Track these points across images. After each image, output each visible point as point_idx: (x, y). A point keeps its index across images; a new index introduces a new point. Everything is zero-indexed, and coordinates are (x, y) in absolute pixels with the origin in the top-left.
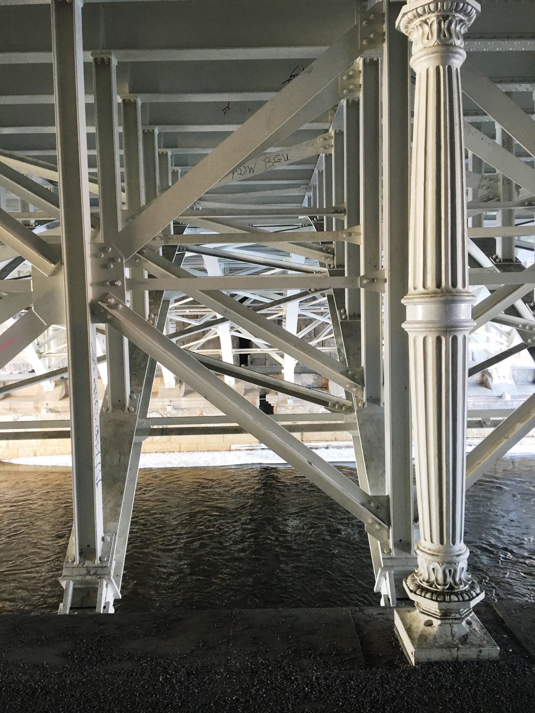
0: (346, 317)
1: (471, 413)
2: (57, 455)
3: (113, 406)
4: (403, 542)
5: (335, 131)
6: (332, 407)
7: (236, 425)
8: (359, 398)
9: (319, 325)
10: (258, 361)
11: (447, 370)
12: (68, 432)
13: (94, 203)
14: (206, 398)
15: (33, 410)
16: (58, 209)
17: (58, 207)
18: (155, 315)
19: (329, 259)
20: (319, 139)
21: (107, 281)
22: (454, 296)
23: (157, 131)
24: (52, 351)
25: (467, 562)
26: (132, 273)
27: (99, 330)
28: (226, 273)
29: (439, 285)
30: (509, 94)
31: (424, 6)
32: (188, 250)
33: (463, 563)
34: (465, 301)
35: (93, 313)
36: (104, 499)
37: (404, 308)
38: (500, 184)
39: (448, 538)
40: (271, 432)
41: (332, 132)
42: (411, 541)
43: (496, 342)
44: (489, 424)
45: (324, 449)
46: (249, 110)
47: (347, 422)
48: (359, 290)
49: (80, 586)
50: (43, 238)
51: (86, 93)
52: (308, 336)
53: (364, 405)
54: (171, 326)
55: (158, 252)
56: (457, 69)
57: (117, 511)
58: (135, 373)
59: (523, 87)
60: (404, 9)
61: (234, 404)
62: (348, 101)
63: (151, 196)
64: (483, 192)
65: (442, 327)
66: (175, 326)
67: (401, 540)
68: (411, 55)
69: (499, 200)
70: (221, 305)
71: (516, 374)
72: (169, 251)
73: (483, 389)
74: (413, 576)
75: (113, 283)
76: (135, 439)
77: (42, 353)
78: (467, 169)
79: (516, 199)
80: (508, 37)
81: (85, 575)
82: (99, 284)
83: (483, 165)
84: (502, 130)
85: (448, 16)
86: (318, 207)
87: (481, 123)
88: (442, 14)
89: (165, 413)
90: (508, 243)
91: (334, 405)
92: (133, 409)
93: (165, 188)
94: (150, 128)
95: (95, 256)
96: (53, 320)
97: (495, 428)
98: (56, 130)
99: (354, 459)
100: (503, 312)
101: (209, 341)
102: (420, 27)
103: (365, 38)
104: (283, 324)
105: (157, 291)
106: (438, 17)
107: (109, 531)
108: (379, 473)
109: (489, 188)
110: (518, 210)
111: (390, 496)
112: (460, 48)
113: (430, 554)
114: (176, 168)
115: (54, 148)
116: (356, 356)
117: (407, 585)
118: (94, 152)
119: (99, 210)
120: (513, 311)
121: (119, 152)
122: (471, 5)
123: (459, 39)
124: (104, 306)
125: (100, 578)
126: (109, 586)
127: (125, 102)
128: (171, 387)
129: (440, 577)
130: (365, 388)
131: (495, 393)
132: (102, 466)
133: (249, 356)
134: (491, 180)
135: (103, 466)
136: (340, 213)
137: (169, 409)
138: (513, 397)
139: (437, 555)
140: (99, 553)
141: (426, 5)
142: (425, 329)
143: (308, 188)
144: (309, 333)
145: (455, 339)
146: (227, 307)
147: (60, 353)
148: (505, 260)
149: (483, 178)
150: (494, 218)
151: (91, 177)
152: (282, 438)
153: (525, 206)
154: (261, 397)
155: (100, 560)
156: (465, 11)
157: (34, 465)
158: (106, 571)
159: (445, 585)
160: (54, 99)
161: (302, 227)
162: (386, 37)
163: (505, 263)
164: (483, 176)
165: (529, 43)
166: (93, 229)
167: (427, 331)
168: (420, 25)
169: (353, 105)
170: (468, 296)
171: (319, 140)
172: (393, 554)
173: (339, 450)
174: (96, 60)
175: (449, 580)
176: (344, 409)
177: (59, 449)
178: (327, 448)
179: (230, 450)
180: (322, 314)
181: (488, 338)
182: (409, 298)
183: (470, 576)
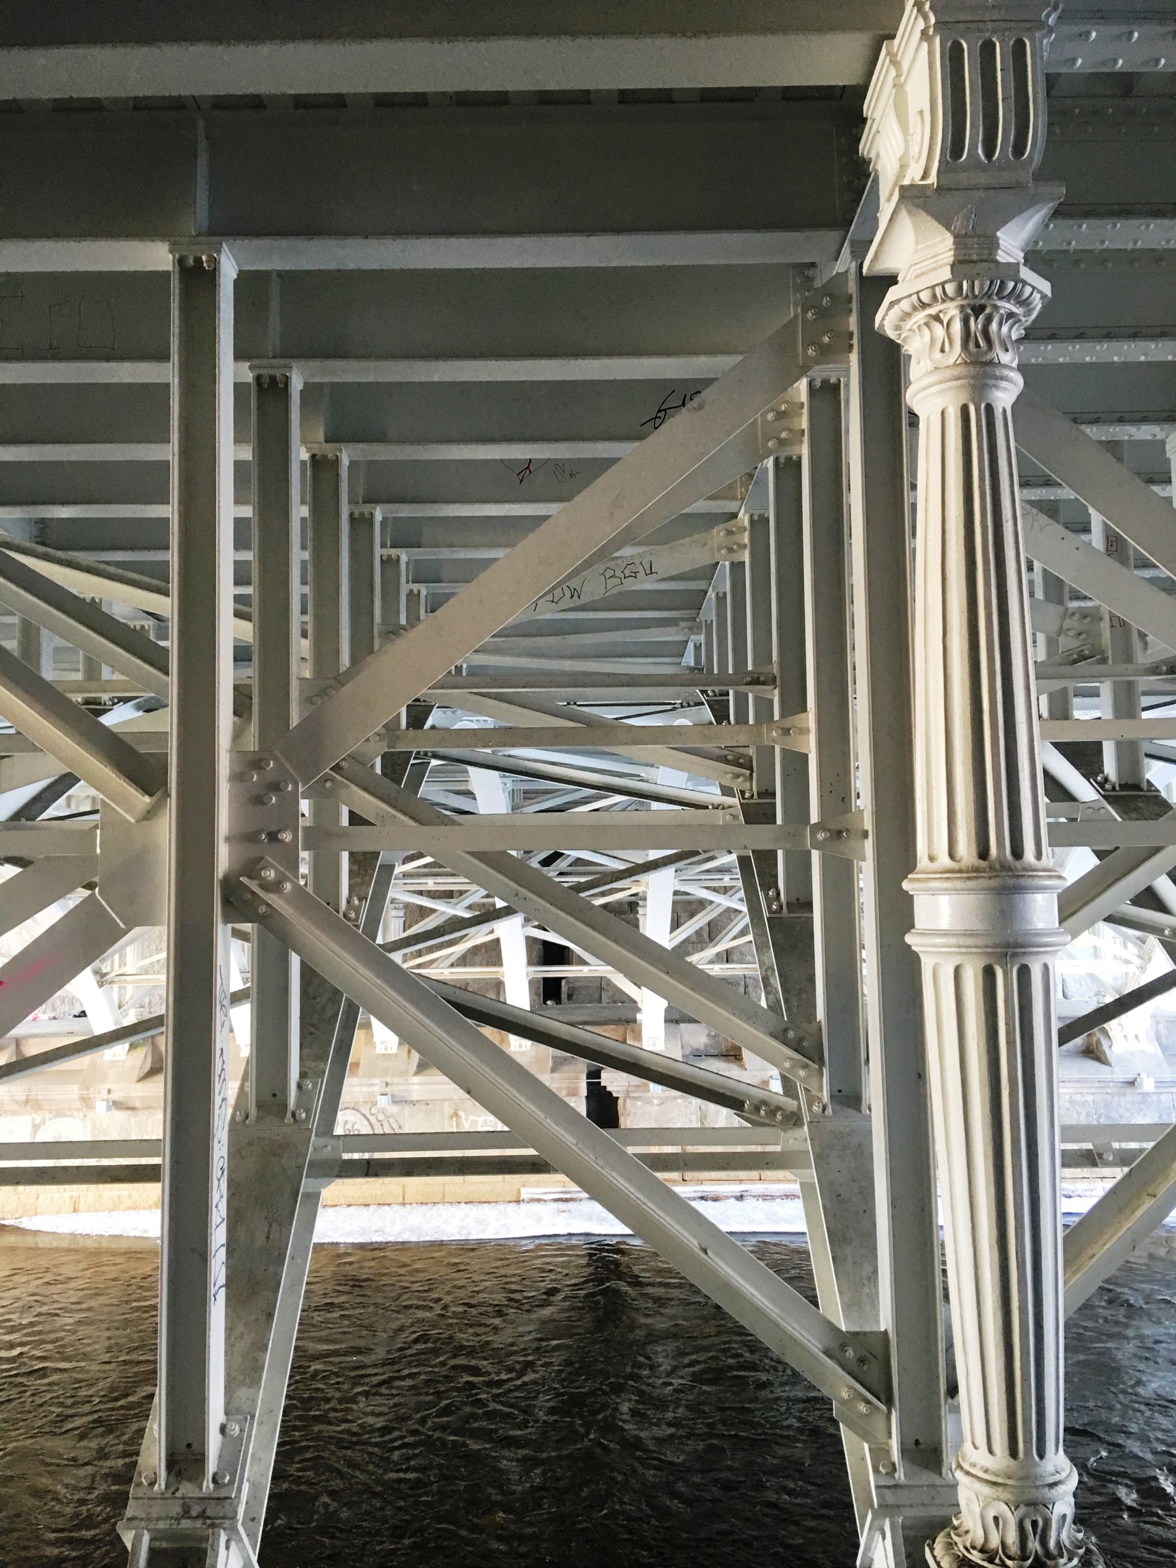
0: (781, 907)
1: (1070, 1133)
2: (124, 1211)
3: (260, 1106)
4: (921, 1447)
5: (752, 516)
6: (752, 1113)
7: (531, 1152)
8: (814, 1092)
9: (720, 915)
10: (584, 993)
11: (1010, 1043)
12: (156, 1168)
13: (241, 655)
14: (468, 1093)
15: (78, 1105)
16: (165, 677)
17: (167, 673)
18: (360, 900)
19: (740, 779)
20: (718, 533)
21: (259, 832)
22: (1018, 876)
23: (378, 516)
24: (128, 969)
25: (1072, 1500)
26: (317, 812)
27: (237, 934)
28: (517, 800)
29: (983, 853)
30: (1113, 447)
31: (933, 287)
32: (436, 756)
33: (1064, 1505)
34: (1044, 889)
35: (227, 901)
36: (229, 1330)
37: (908, 900)
38: (1105, 625)
39: (1027, 1442)
40: (614, 1174)
41: (744, 518)
42: (940, 1443)
43: (1115, 957)
44: (1111, 1158)
45: (733, 1200)
46: (571, 475)
47: (789, 1149)
48: (808, 855)
49: (164, 1545)
50: (127, 739)
51: (237, 441)
52: (694, 939)
53: (824, 1109)
54: (393, 913)
55: (373, 766)
56: (1004, 411)
57: (257, 1360)
58: (313, 1030)
59: (1146, 432)
60: (892, 293)
61: (532, 1107)
62: (777, 460)
63: (363, 648)
64: (1067, 643)
65: (995, 946)
66: (402, 913)
67: (917, 1442)
68: (908, 383)
69: (1104, 661)
70: (506, 880)
71: (1164, 1032)
72: (395, 764)
73: (1092, 1065)
74: (949, 1535)
75: (273, 837)
76: (306, 1185)
77: (106, 974)
78: (1032, 594)
79: (1143, 658)
80: (1109, 335)
81: (178, 1519)
82: (244, 838)
83: (1067, 590)
84: (1105, 524)
85: (983, 308)
86: (716, 671)
87: (1056, 502)
88: (972, 302)
89: (373, 1111)
90: (1130, 754)
91: (757, 1109)
92: (304, 1115)
93: (393, 632)
94: (366, 509)
95: (237, 777)
96: (140, 917)
97: (1126, 1170)
98: (170, 511)
99: (802, 1227)
100: (1129, 902)
101: (476, 949)
102: (925, 329)
103: (814, 344)
104: (641, 911)
105: (365, 854)
106: (962, 308)
107: (238, 1411)
108: (864, 1274)
109: (1080, 634)
110: (1146, 682)
111: (891, 1334)
112: (1011, 368)
113: (987, 1482)
114: (415, 587)
115: (166, 547)
116: (804, 996)
117: (934, 1557)
118: (248, 556)
119: (251, 672)
120: (1150, 898)
121: (299, 555)
122: (1030, 285)
123: (1007, 350)
124: (253, 885)
125: (213, 1526)
126: (233, 1545)
127: (317, 461)
128: (389, 1051)
129: (1012, 1537)
130: (825, 1071)
131: (1120, 1074)
132: (227, 1253)
133: (563, 982)
134: (1085, 617)
135: (230, 1252)
136: (764, 683)
137: (383, 1102)
138: (1160, 1083)
139: (1004, 1485)
140: (212, 1466)
141: (937, 285)
142: (957, 950)
143: (694, 628)
144: (698, 933)
145: (1024, 972)
146: (520, 885)
147: (147, 973)
148: (1123, 787)
149: (1067, 614)
150: (1095, 693)
151: (241, 607)
152: (639, 1189)
153: (1159, 674)
154: (589, 1076)
155: (215, 1481)
156: (1019, 296)
157: (72, 1234)
158: (228, 1510)
159: (1024, 1558)
160: (170, 452)
161: (682, 707)
162: (855, 342)
163: (1125, 793)
164: (1067, 609)
165: (1153, 346)
166: (236, 719)
167: (961, 953)
168: (927, 324)
169: (789, 469)
170: (1050, 877)
171: (718, 534)
172: (900, 1475)
173: (768, 1203)
174: (258, 379)
175: (1034, 1545)
176: (779, 1117)
177: (130, 1196)
178: (740, 1198)
179: (518, 1202)
180: (725, 890)
181: (1095, 948)
182: (919, 880)
183: (1080, 1536)
